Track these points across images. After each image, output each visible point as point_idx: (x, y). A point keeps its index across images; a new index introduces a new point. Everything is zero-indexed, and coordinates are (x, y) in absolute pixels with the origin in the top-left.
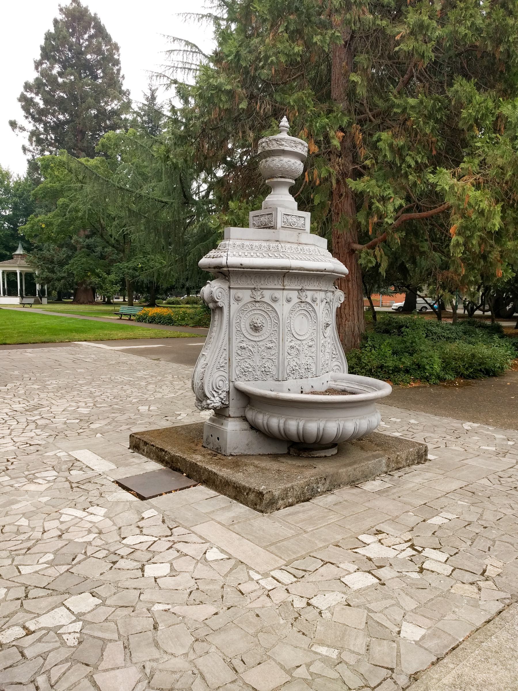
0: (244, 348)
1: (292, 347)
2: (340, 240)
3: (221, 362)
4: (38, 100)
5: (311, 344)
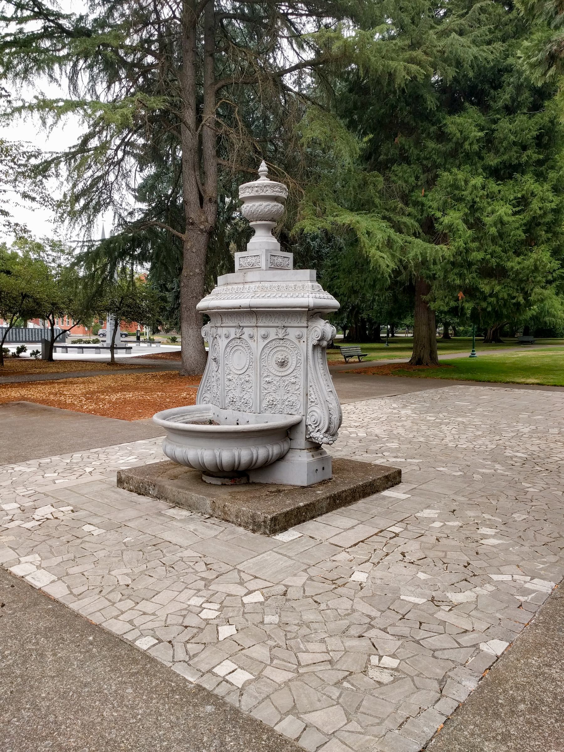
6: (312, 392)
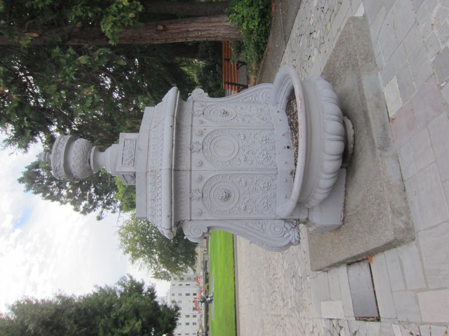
0: (246, 207)
1: (243, 120)
2: (155, 38)
3: (257, 228)
4: (84, 203)
5: (242, 137)
6: (247, 100)
